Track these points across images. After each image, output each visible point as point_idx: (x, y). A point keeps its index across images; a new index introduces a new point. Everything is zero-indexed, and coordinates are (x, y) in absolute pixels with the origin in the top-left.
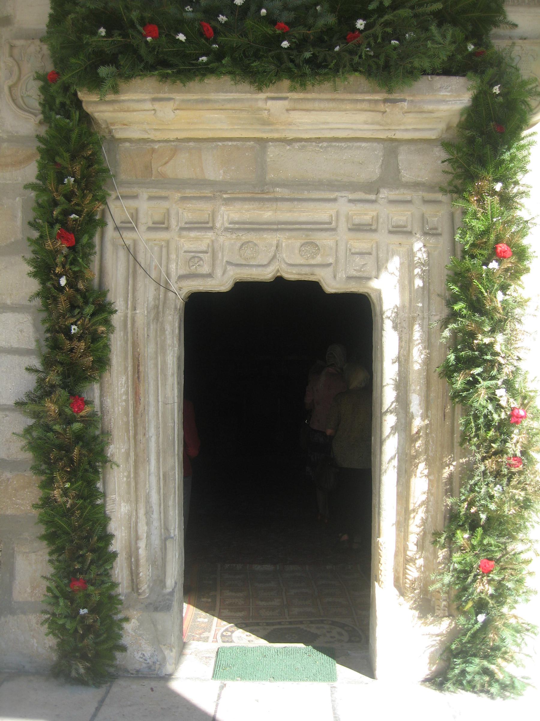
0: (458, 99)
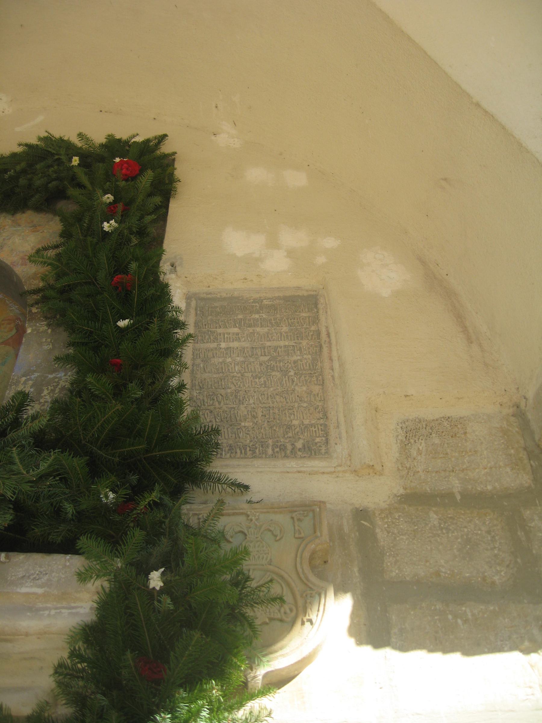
0: (64, 604)
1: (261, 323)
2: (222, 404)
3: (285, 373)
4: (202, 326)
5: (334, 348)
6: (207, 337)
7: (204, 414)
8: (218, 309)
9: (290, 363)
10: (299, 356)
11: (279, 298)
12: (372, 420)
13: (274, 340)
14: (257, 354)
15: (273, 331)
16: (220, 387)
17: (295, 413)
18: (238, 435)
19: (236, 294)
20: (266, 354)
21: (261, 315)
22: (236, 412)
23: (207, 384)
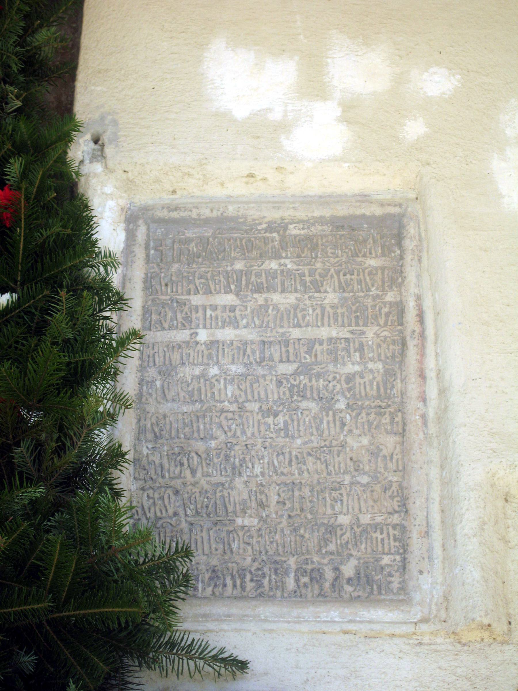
1: (283, 283)
2: (199, 475)
3: (327, 403)
4: (158, 287)
5: (430, 349)
6: (170, 314)
7: (162, 498)
8: (193, 245)
9: (339, 382)
10: (358, 363)
11: (321, 220)
12: (497, 522)
13: (307, 326)
14: (271, 359)
15: (307, 302)
16: (196, 435)
17: (345, 499)
18: (229, 544)
19: (231, 211)
20: (292, 358)
21: (282, 261)
22: (226, 495)
23: (168, 427)
